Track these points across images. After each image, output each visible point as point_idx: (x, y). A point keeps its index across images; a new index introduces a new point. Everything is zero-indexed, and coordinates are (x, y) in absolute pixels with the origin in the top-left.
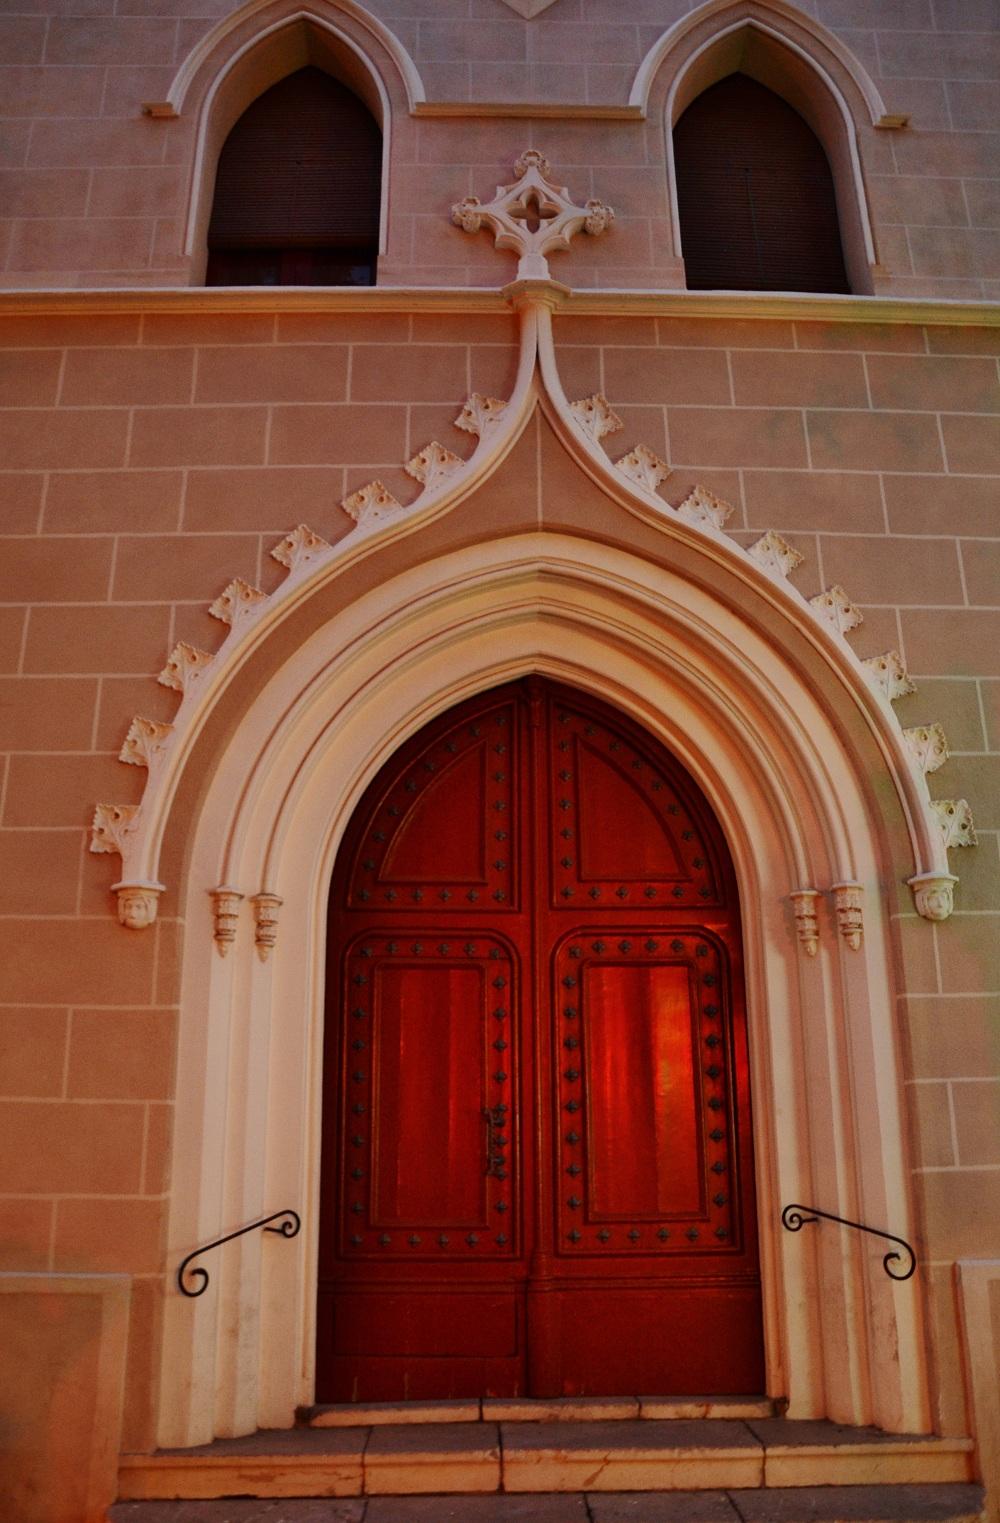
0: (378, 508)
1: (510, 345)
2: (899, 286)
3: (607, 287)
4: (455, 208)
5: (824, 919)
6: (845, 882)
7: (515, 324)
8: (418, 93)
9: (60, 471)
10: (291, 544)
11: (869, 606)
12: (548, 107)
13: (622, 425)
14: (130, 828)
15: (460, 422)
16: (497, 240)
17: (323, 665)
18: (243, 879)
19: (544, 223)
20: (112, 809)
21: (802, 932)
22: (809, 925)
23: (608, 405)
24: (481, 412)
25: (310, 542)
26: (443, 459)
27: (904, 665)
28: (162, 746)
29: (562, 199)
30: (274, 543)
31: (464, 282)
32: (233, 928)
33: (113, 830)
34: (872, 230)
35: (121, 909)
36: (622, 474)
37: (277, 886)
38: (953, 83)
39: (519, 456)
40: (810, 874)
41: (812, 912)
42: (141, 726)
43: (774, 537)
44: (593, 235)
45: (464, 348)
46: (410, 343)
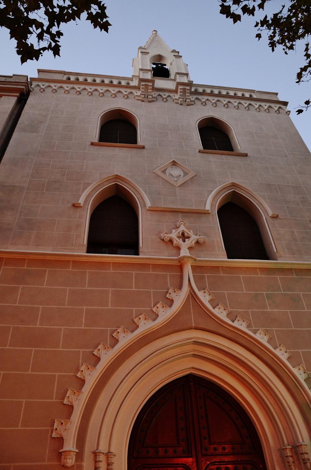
0: (145, 322)
1: (179, 274)
2: (284, 259)
3: (205, 258)
4: (162, 235)
5: (295, 457)
6: (301, 443)
7: (181, 268)
8: (149, 204)
9: (45, 306)
10: (119, 332)
11: (291, 350)
12: (185, 209)
13: (214, 297)
14: (67, 428)
15: (168, 296)
16: (174, 244)
17: (129, 371)
18: (103, 448)
19: (187, 240)
20: (61, 421)
21: (288, 462)
22: (291, 459)
23: (210, 291)
24: (173, 293)
25: (125, 332)
26: (163, 307)
27: (305, 369)
28: (79, 398)
29: (191, 233)
30: (114, 331)
31: (165, 255)
32: (101, 466)
33: (60, 428)
34: (274, 243)
35: (62, 460)
36: (216, 311)
37: (112, 450)
38: (287, 207)
39: (186, 306)
40: (287, 440)
41: (291, 455)
42: (71, 391)
43: (262, 330)
44: (200, 243)
45: (167, 274)
46: (151, 272)
